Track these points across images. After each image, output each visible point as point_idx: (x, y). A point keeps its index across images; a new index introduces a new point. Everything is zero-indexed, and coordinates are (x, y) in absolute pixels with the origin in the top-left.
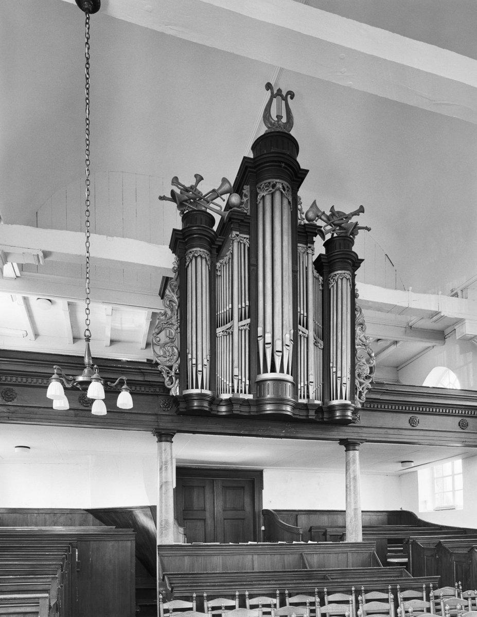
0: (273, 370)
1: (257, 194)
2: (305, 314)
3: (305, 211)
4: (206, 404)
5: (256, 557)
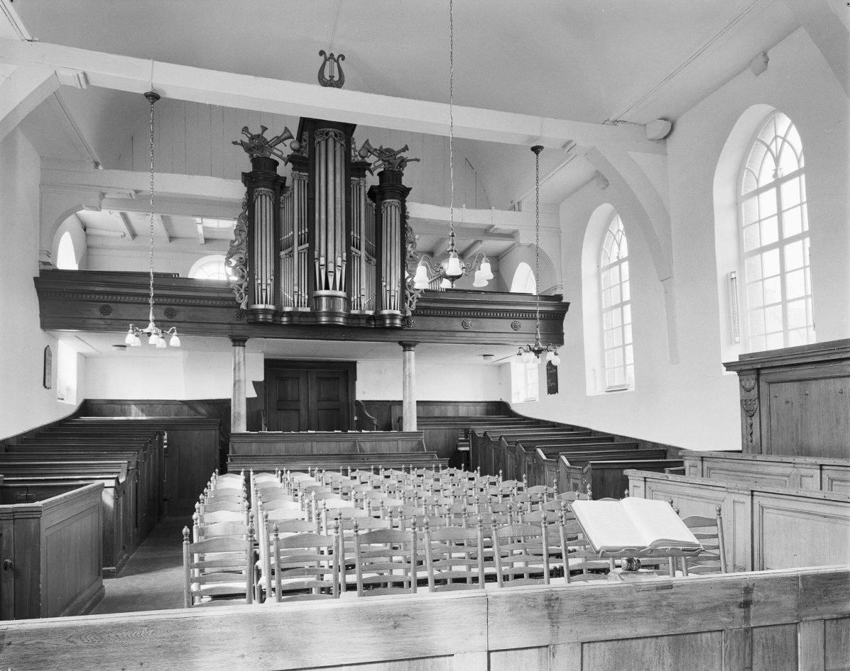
1: (315, 139)
2: (358, 237)
3: (358, 149)
4: (270, 317)
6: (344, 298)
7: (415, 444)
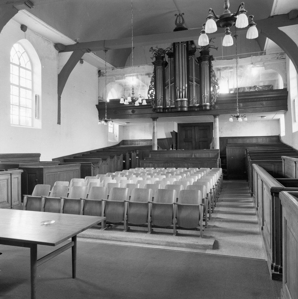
0: (180, 98)
5: (178, 154)
6: (187, 101)
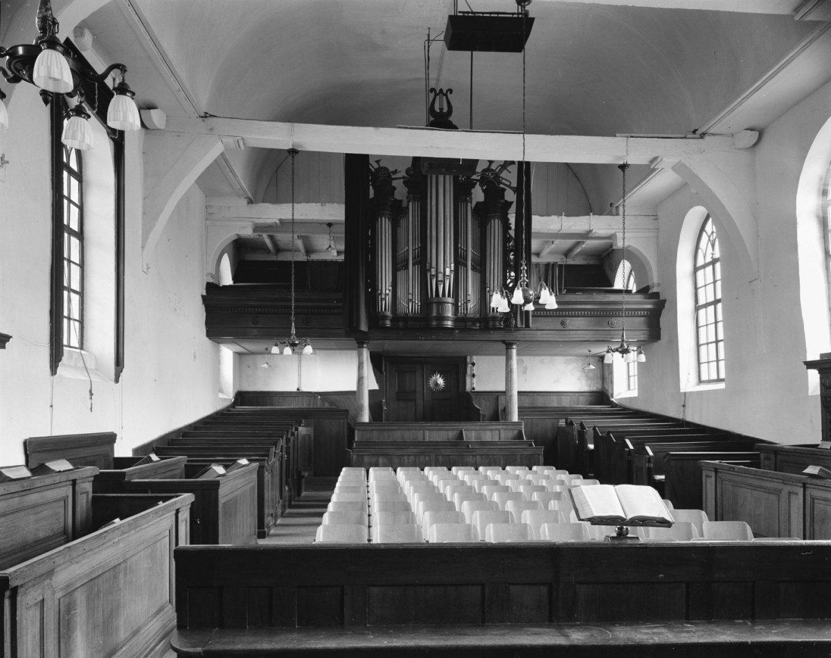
7: (516, 432)
